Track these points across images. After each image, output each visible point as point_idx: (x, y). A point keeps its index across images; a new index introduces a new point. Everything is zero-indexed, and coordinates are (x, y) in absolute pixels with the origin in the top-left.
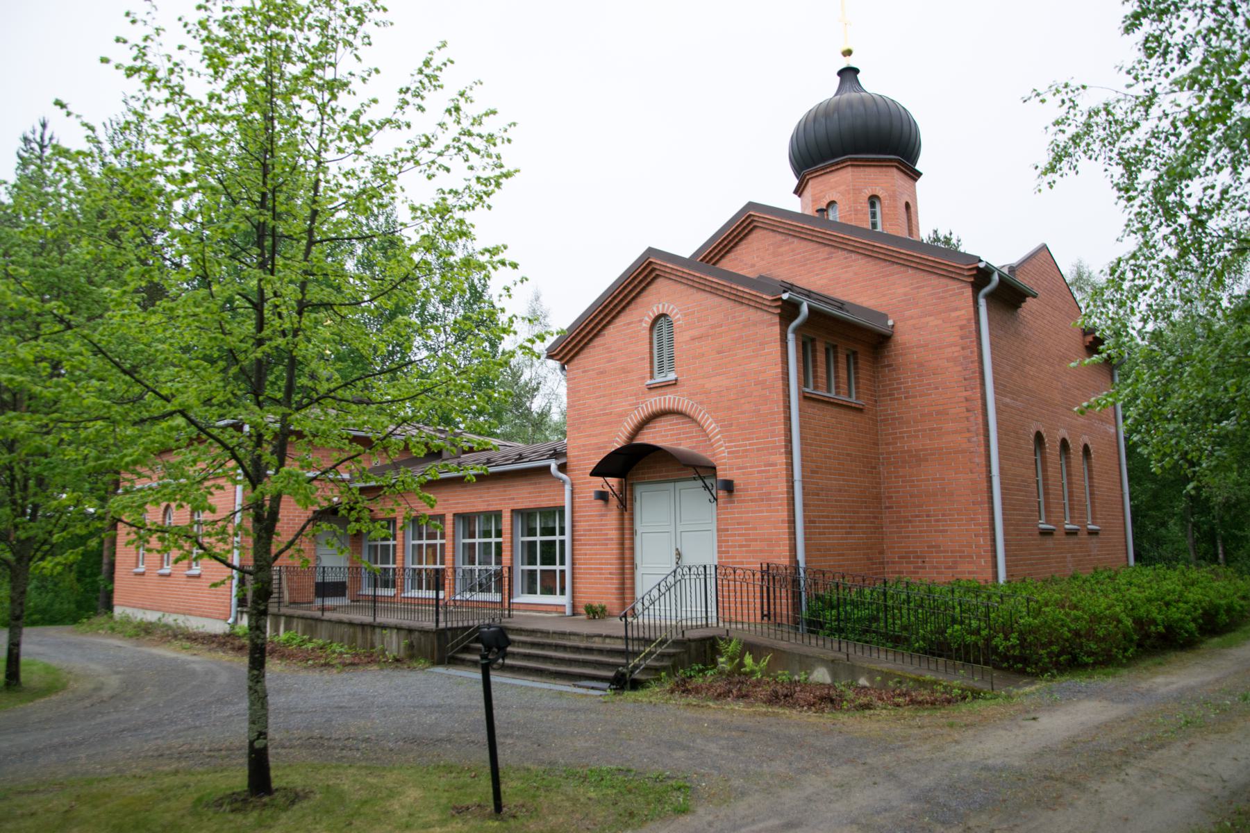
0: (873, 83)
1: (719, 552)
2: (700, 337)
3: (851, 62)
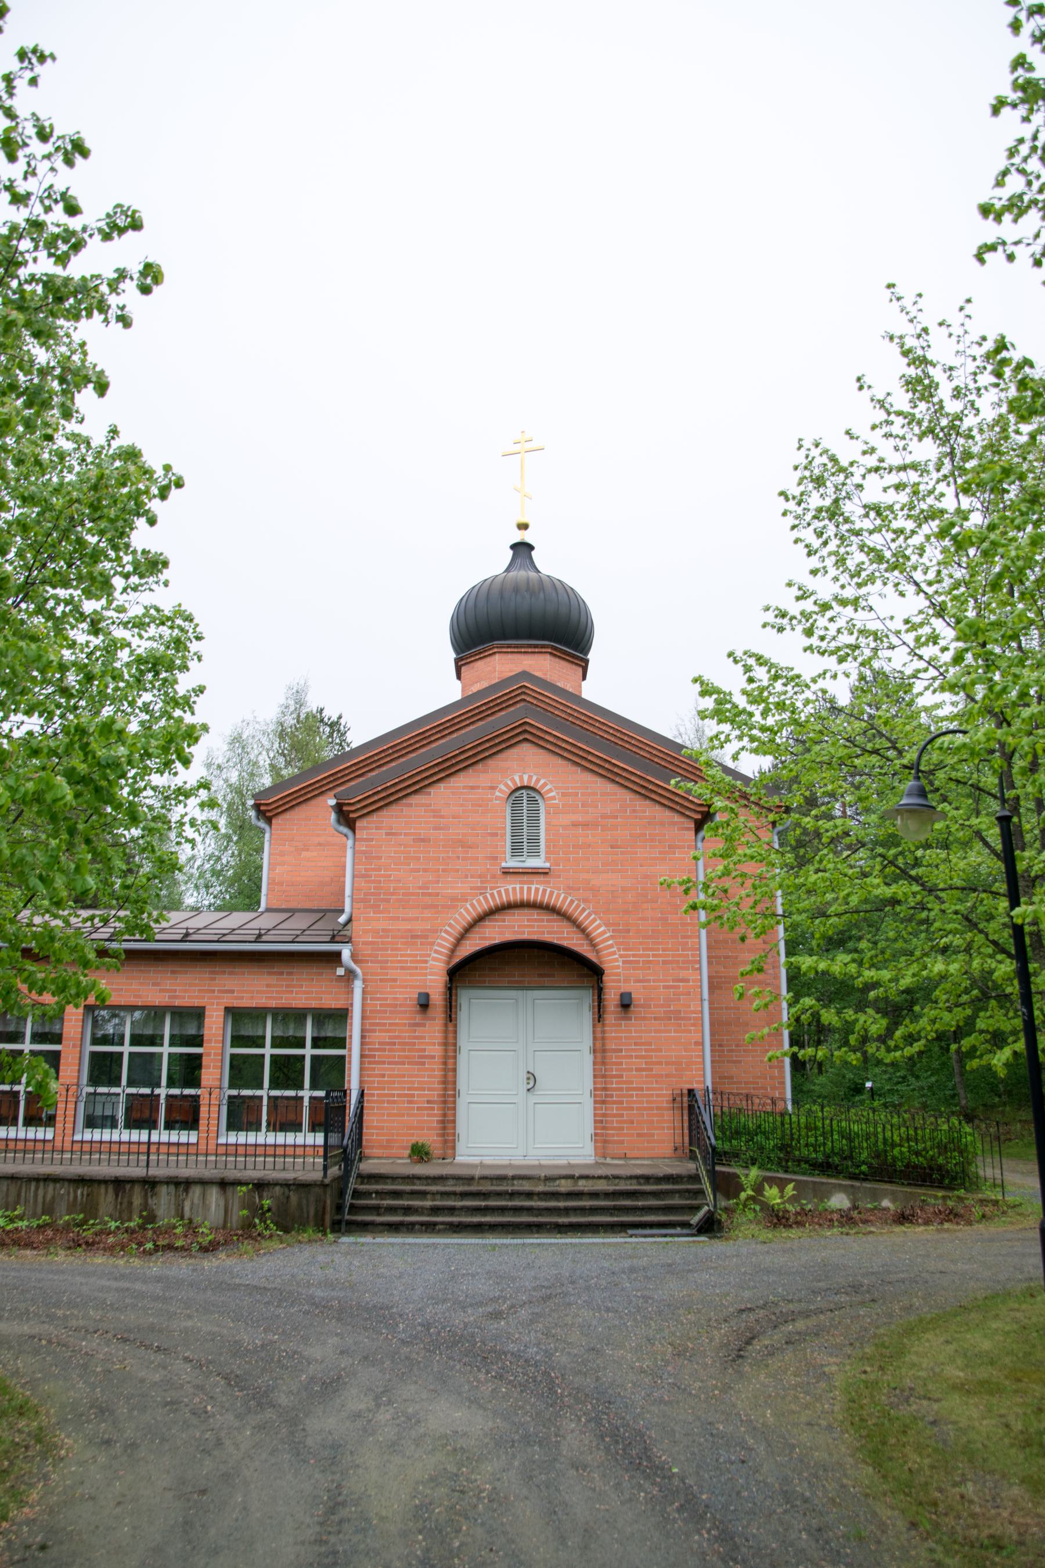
0: (549, 563)
1: (595, 1076)
2: (585, 825)
3: (527, 537)
